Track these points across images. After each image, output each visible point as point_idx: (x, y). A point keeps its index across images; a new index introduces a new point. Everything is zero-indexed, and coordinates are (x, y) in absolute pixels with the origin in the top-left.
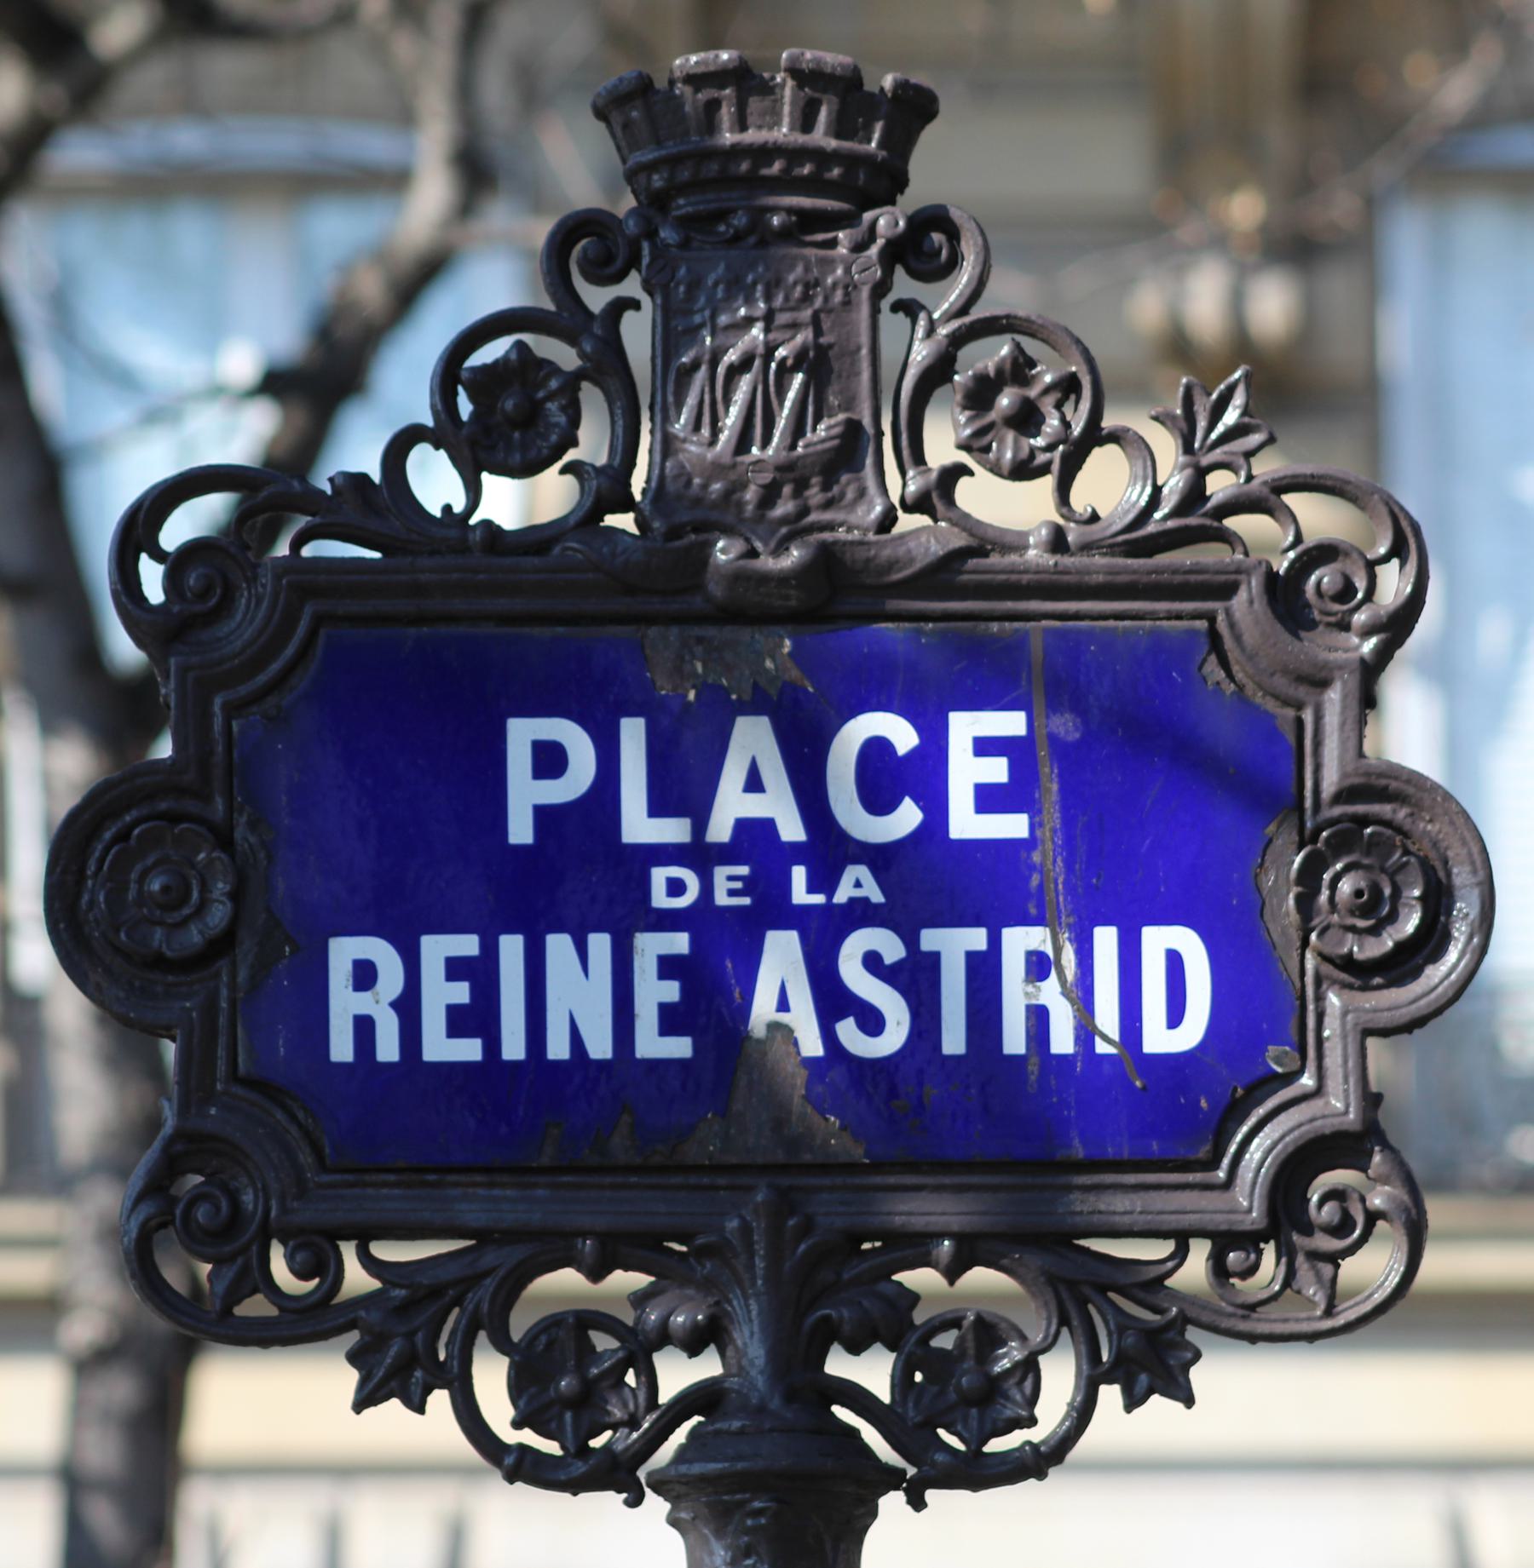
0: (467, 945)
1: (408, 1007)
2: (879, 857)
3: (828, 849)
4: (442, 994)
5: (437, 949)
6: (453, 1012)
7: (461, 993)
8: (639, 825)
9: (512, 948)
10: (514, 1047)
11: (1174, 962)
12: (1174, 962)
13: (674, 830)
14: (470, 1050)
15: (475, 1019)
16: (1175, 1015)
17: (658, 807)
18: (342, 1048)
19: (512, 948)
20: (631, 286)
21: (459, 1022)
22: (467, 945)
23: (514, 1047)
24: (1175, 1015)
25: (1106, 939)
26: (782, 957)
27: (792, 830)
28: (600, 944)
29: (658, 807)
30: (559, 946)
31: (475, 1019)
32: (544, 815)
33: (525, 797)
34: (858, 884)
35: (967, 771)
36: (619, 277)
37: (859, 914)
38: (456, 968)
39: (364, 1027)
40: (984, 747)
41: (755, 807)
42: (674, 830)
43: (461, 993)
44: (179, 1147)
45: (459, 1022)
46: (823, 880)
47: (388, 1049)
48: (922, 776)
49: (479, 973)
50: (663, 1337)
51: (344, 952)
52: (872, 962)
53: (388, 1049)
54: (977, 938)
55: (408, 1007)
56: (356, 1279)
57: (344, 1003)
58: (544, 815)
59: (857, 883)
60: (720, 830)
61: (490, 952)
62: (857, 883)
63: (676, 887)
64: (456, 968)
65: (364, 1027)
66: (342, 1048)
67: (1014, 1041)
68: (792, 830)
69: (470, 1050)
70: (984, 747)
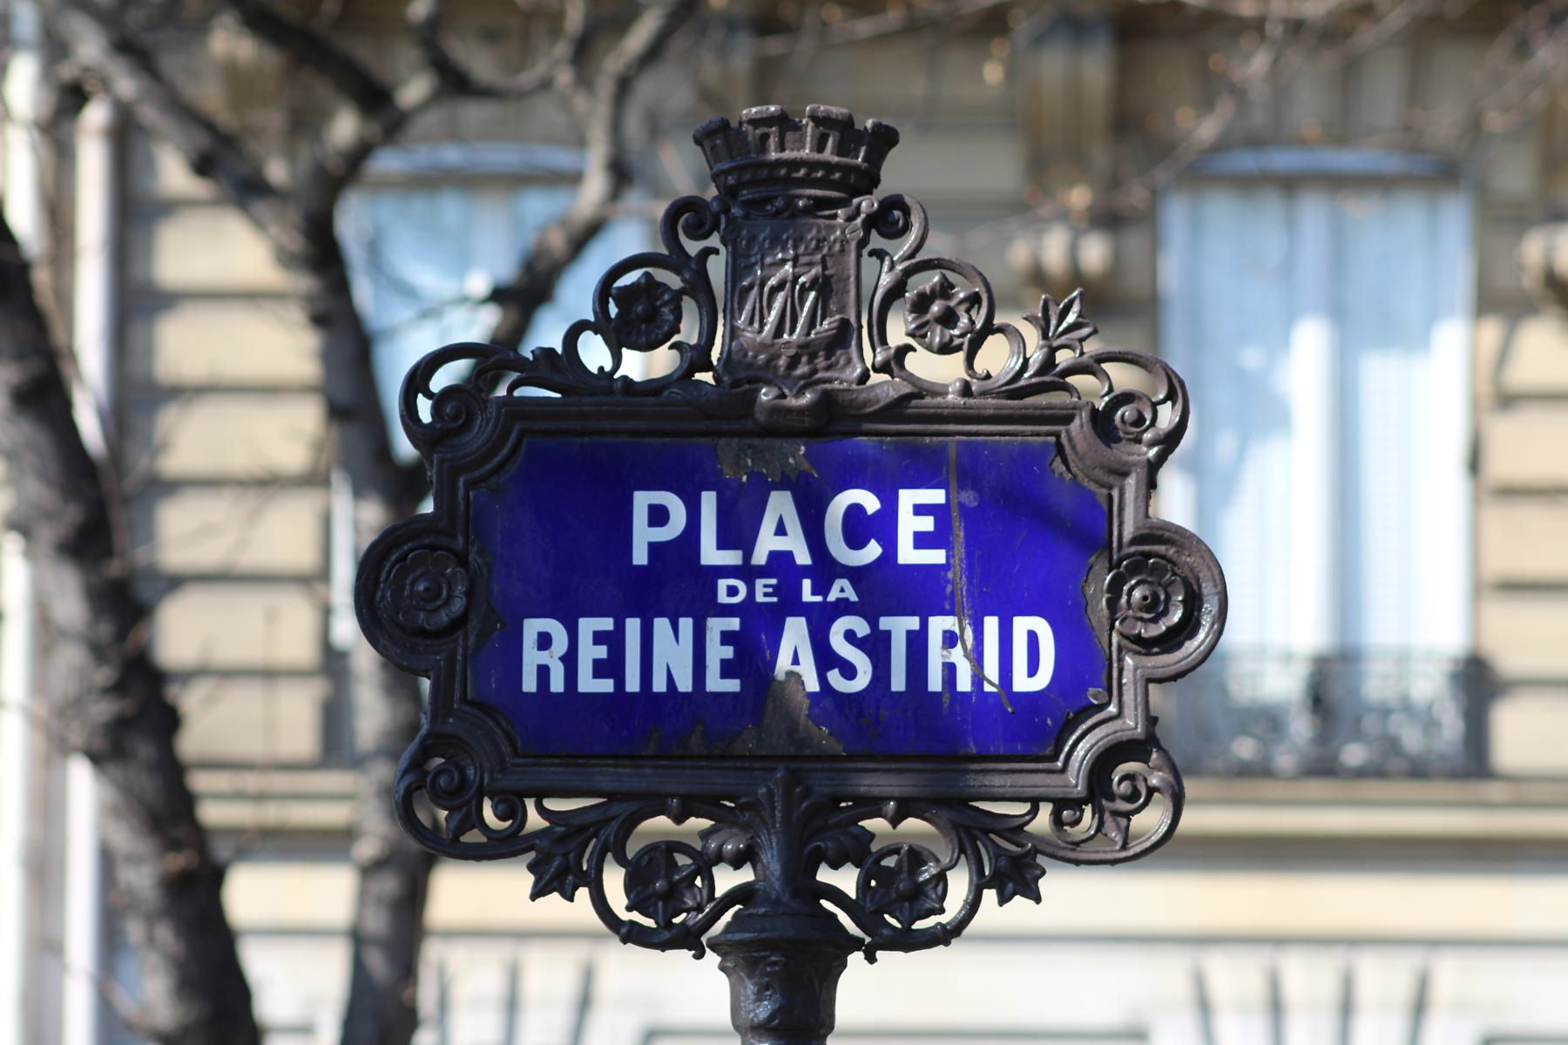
0: (607, 624)
1: (570, 660)
2: (856, 575)
3: (825, 569)
4: (590, 653)
5: (588, 626)
6: (724, 663)
7: (602, 652)
8: (711, 554)
9: (633, 626)
10: (633, 684)
11: (1033, 638)
12: (1033, 638)
13: (732, 558)
14: (606, 686)
15: (610, 667)
16: (1033, 669)
17: (722, 544)
18: (530, 684)
19: (633, 626)
20: (714, 241)
21: (600, 669)
22: (607, 624)
23: (633, 684)
24: (1033, 669)
25: (991, 624)
26: (795, 633)
27: (803, 558)
28: (686, 624)
29: (722, 544)
30: (661, 625)
31: (610, 667)
32: (654, 548)
33: (643, 536)
34: (842, 590)
35: (909, 524)
36: (707, 236)
37: (843, 607)
38: (599, 638)
39: (543, 672)
40: (919, 510)
41: (781, 544)
42: (732, 558)
43: (602, 652)
44: (430, 742)
45: (600, 669)
46: (821, 588)
47: (557, 684)
48: (883, 526)
49: (613, 640)
50: (719, 858)
51: (532, 627)
52: (850, 636)
53: (557, 684)
54: (913, 623)
55: (570, 660)
56: (534, 820)
57: (532, 657)
58: (654, 548)
59: (842, 589)
60: (760, 558)
61: (620, 628)
62: (842, 589)
63: (732, 591)
64: (599, 638)
65: (543, 672)
66: (530, 684)
67: (935, 683)
68: (803, 558)
69: (606, 686)
70: (919, 510)
